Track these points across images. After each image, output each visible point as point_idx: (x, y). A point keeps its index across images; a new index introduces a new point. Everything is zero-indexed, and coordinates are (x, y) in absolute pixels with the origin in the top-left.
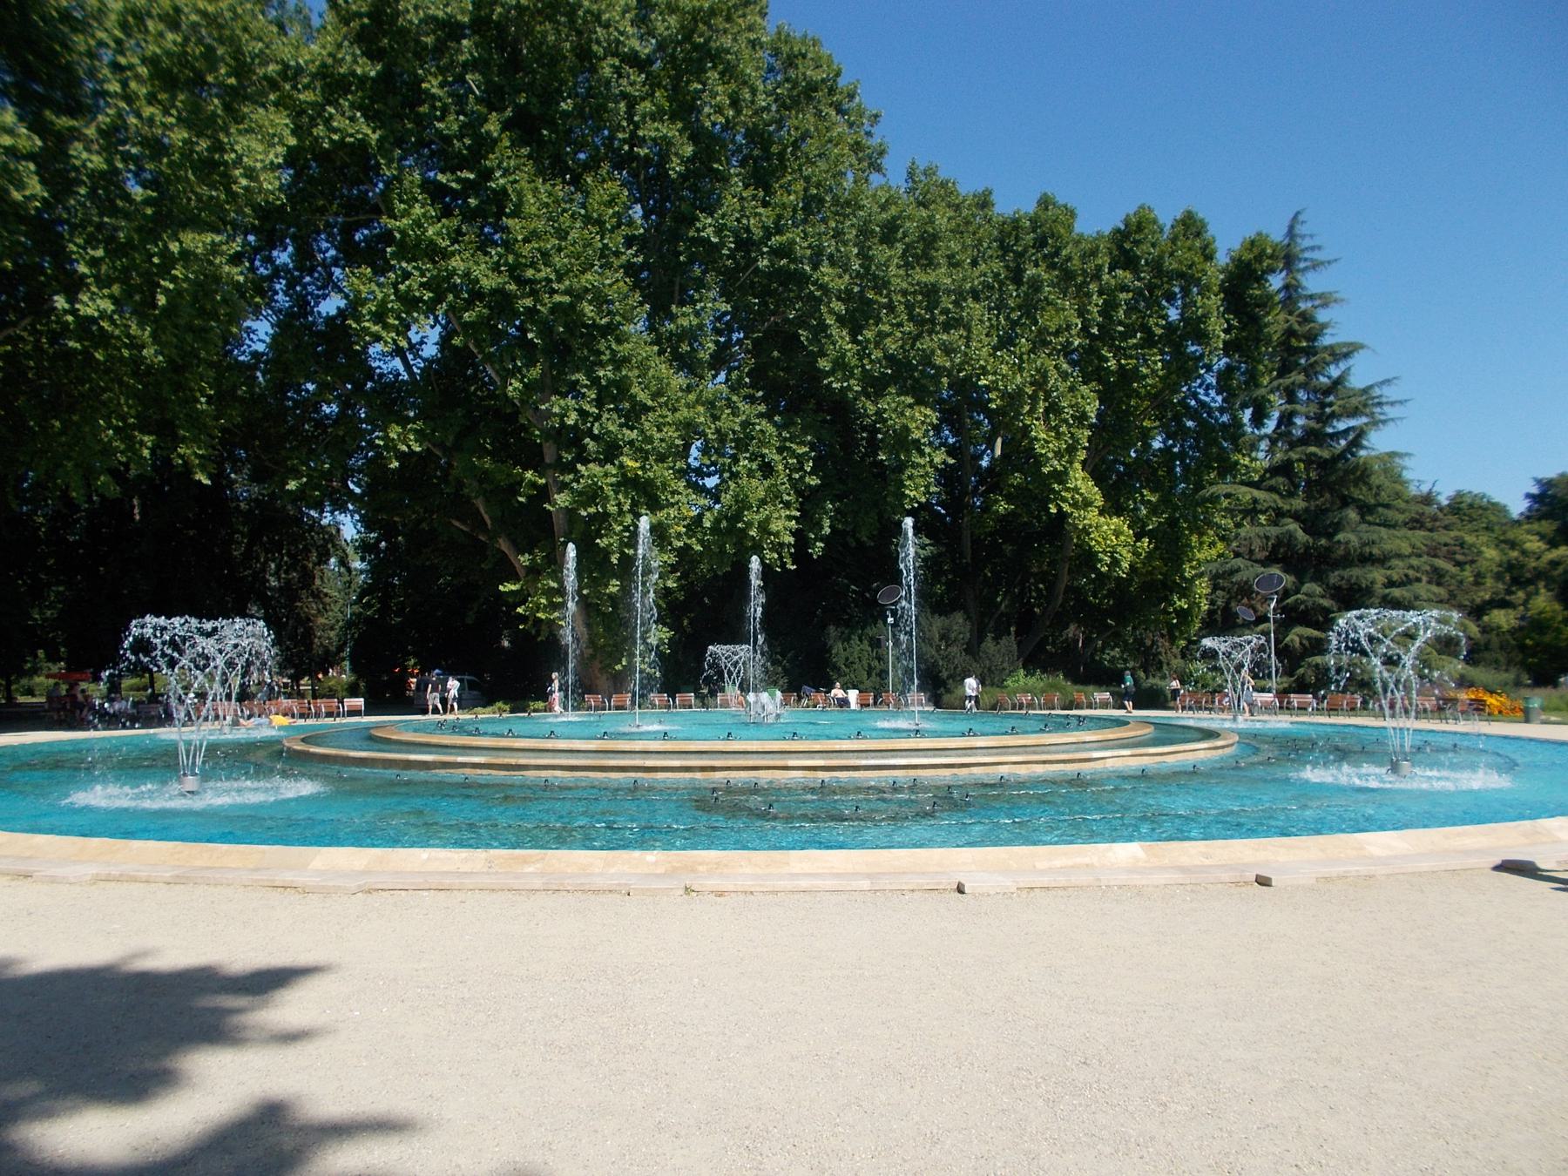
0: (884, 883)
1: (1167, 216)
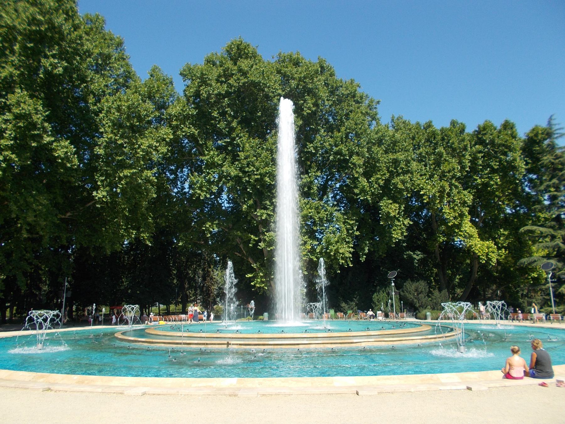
1: (498, 124)
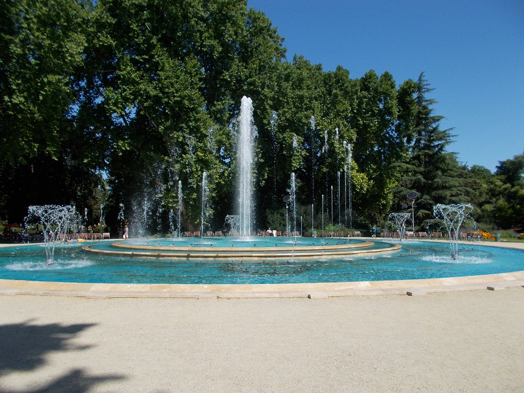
0: (284, 295)
1: (379, 73)
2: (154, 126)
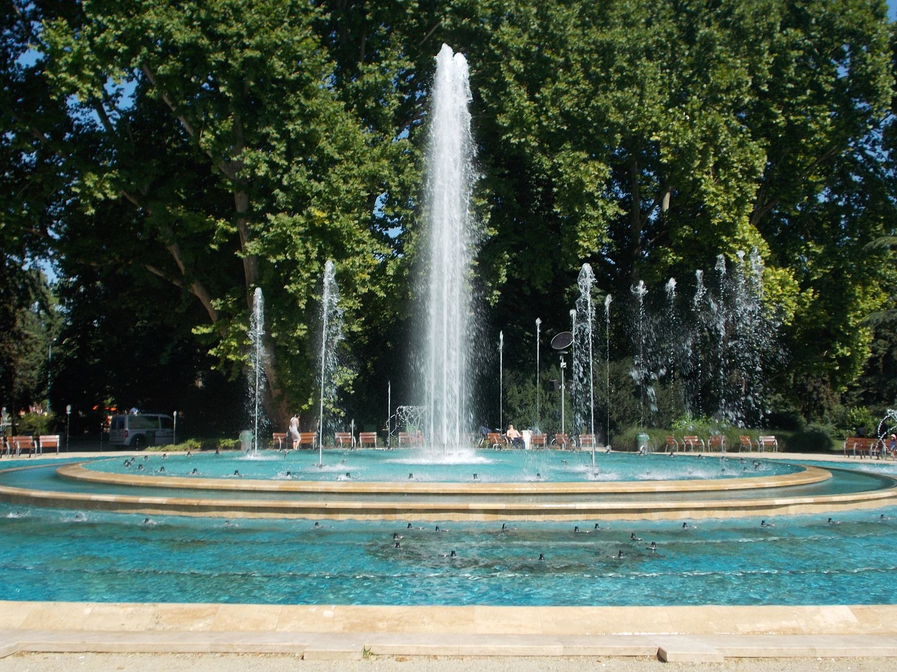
0: (578, 648)
2: (186, 134)
